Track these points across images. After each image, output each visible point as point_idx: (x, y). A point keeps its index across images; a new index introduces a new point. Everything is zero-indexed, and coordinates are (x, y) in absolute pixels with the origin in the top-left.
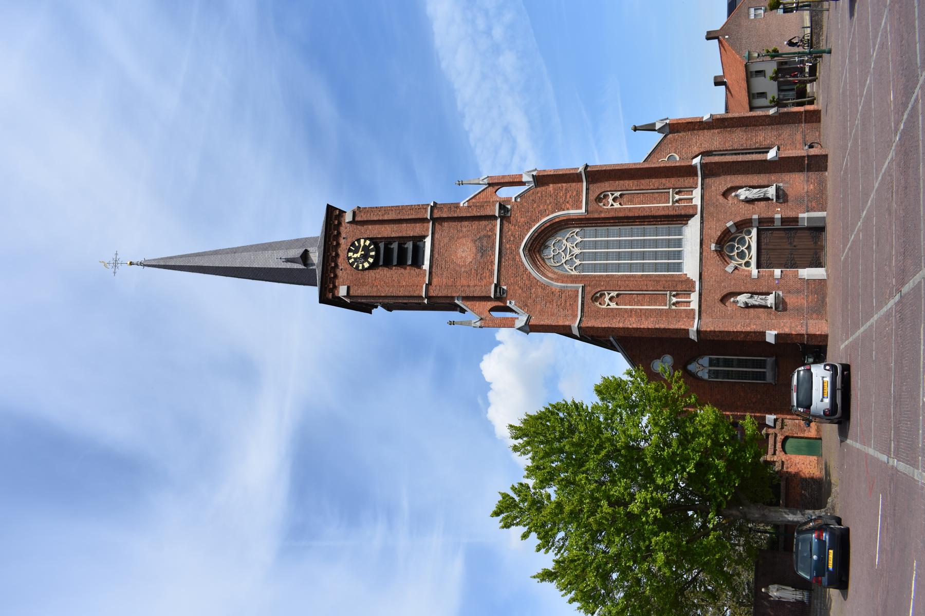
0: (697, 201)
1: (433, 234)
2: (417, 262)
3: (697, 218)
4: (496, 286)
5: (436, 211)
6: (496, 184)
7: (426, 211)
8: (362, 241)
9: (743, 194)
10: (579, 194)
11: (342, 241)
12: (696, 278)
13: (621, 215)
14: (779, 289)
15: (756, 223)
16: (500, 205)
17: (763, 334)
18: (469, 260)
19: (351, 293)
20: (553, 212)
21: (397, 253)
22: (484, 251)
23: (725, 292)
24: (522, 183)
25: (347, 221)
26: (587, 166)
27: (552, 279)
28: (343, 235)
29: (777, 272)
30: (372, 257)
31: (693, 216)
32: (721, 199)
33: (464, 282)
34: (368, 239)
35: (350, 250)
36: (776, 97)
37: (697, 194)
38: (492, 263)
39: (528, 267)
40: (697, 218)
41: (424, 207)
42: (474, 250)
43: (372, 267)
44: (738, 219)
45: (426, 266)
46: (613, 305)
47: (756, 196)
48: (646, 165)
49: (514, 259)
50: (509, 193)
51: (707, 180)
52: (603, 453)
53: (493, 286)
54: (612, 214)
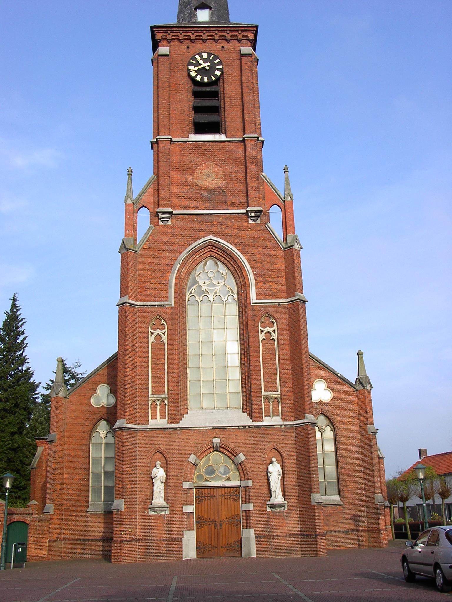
0: (267, 421)
1: (229, 141)
2: (200, 128)
3: (248, 422)
4: (171, 213)
5: (253, 143)
6: (286, 209)
7: (251, 133)
8: (220, 67)
9: (275, 469)
10: (274, 295)
11: (219, 45)
12: (183, 423)
13: (251, 341)
14: (172, 511)
15: (244, 484)
16: (261, 211)
17: (121, 496)
18: (201, 183)
19: (161, 59)
20: (253, 269)
21: (208, 107)
22: (213, 198)
23: (168, 454)
24: (286, 232)
25: (242, 49)
26: (305, 302)
27: (179, 271)
28: (226, 45)
29: (191, 509)
30: (202, 79)
31: (251, 418)
32: (271, 446)
33: (176, 178)
34: (222, 73)
35: (209, 55)
36: (269, 224)
37: (275, 421)
38: (197, 208)
39: (191, 247)
40: (248, 422)
41: (257, 129)
42: (211, 186)
43: (193, 80)
44: (248, 466)
45: (194, 137)
46: (152, 339)
47: (272, 483)
48: (304, 356)
49: (201, 230)
50: (275, 224)
51: (292, 431)
52: (176, 598)
53: (170, 210)
54: (251, 331)
